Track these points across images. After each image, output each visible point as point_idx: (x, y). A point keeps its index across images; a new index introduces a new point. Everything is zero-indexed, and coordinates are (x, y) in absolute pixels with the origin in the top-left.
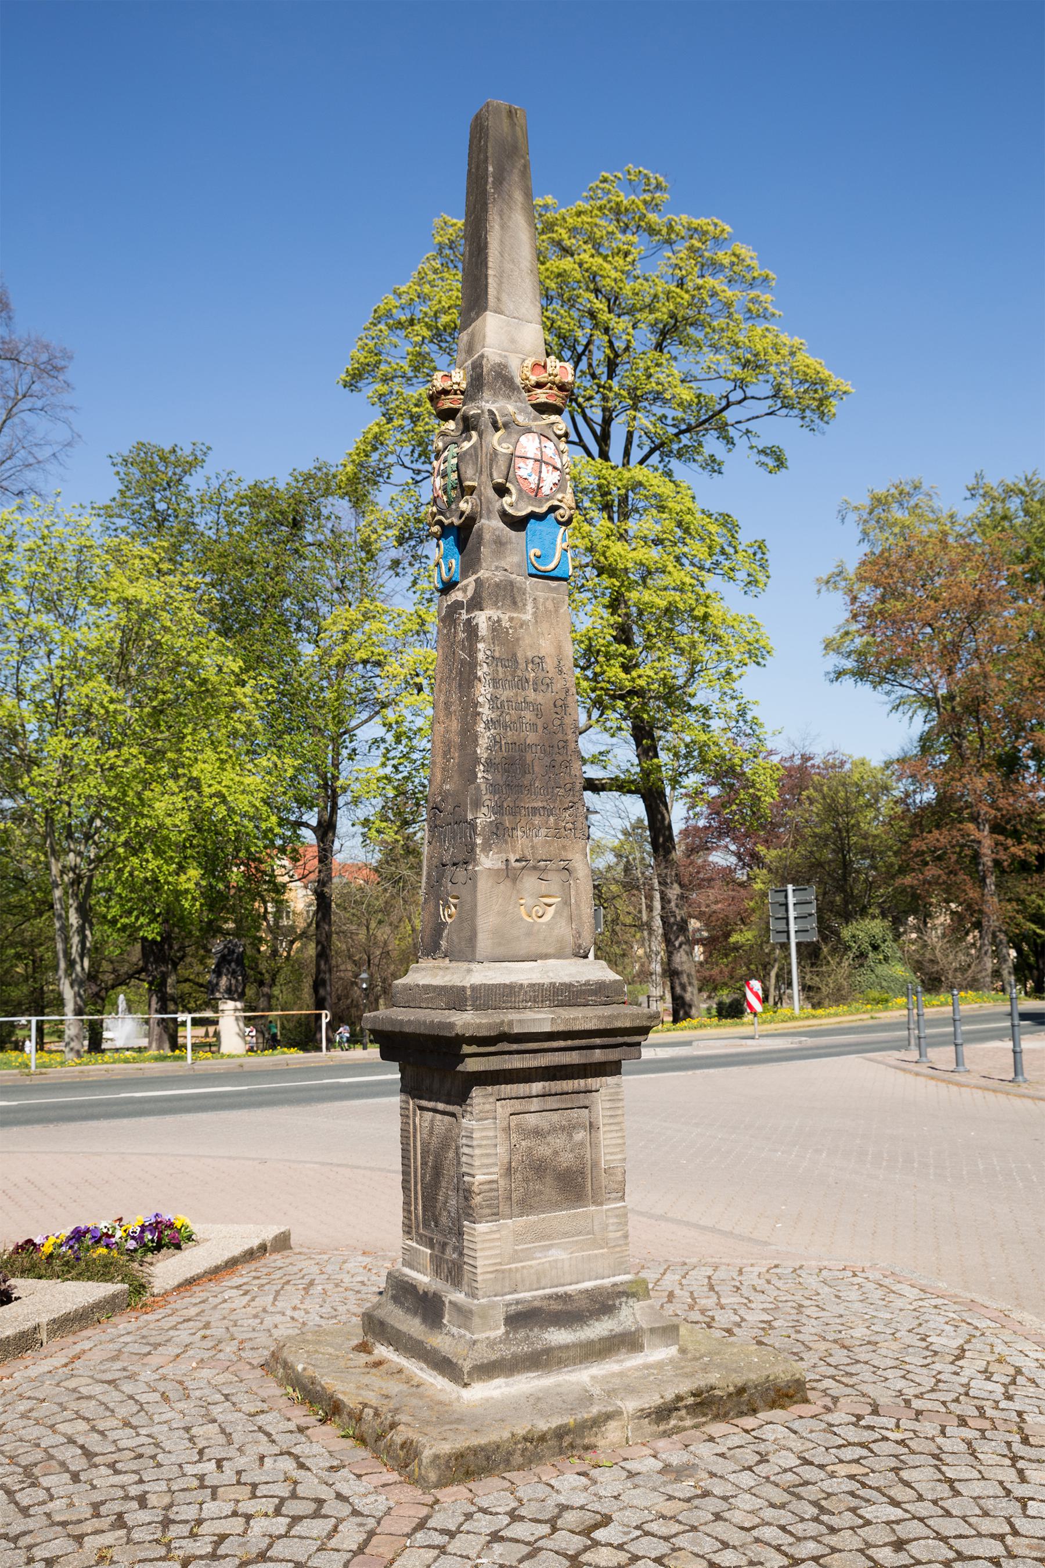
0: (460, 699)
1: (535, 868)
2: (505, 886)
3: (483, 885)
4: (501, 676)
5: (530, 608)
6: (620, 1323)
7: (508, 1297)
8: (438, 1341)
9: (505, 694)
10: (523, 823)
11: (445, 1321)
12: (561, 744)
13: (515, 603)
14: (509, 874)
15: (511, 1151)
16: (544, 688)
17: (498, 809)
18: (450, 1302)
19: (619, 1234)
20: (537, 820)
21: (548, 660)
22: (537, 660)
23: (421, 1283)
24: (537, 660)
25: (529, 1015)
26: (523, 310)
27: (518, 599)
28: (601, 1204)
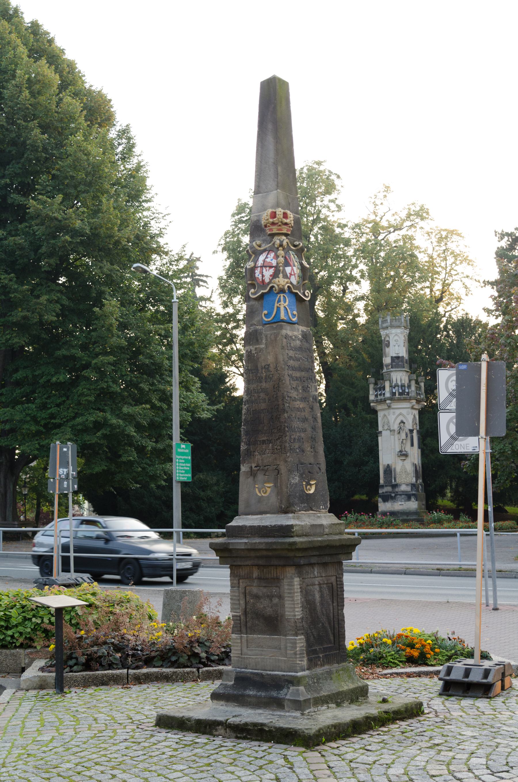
1: (263, 470)
2: (250, 480)
3: (242, 479)
10: (258, 448)
13: (257, 340)
14: (252, 474)
17: (248, 444)
19: (292, 652)
21: (271, 366)
22: (267, 367)
28: (286, 636)
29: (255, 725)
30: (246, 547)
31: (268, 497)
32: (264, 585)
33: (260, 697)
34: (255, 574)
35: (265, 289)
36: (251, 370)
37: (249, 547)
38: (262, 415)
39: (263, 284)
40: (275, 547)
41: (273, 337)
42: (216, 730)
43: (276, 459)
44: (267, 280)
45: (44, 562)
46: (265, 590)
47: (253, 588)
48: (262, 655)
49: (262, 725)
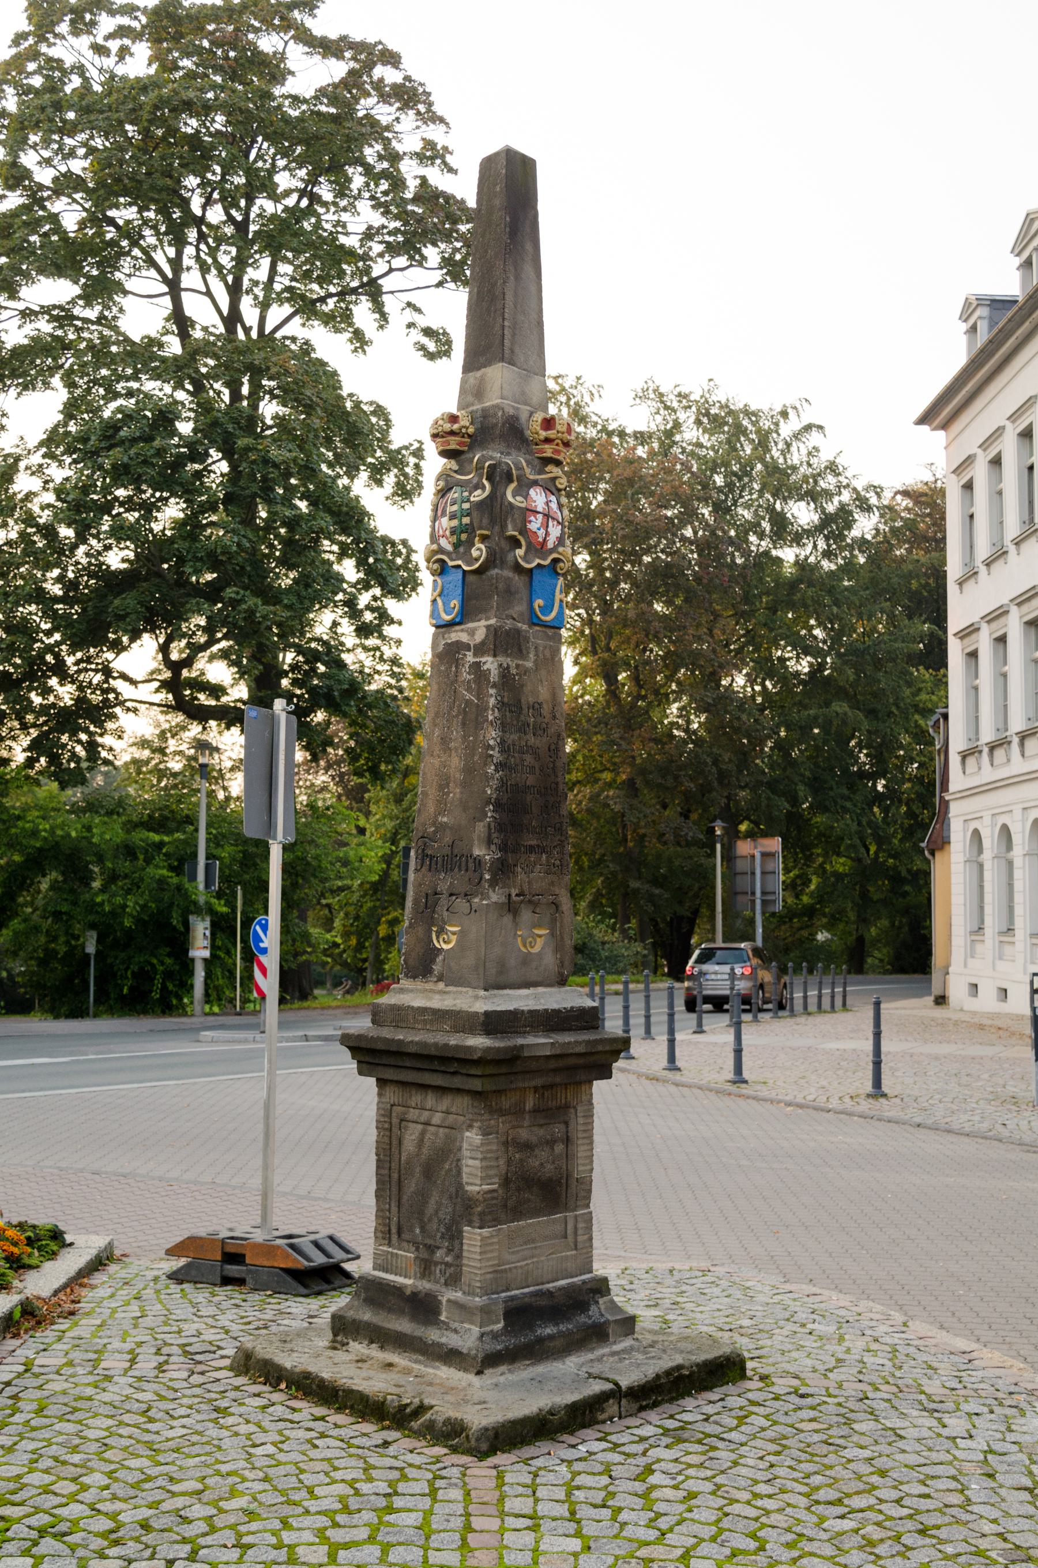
0: (465, 738)
1: (530, 902)
6: (590, 1317)
7: (503, 1295)
8: (433, 1335)
9: (512, 737)
11: (443, 1318)
13: (520, 651)
15: (509, 1162)
18: (449, 1301)
20: (533, 857)
21: (545, 706)
23: (406, 1286)
25: (530, 1040)
28: (575, 1210)
29: (668, 1373)
30: (553, 1052)
31: (539, 954)
32: (542, 1122)
33: (570, 1333)
34: (529, 1104)
35: (544, 559)
36: (509, 705)
37: (558, 1052)
38: (529, 798)
39: (539, 548)
40: (600, 1048)
42: (603, 1411)
43: (552, 883)
44: (550, 545)
46: (541, 1132)
47: (520, 1130)
48: (533, 1257)
49: (679, 1367)
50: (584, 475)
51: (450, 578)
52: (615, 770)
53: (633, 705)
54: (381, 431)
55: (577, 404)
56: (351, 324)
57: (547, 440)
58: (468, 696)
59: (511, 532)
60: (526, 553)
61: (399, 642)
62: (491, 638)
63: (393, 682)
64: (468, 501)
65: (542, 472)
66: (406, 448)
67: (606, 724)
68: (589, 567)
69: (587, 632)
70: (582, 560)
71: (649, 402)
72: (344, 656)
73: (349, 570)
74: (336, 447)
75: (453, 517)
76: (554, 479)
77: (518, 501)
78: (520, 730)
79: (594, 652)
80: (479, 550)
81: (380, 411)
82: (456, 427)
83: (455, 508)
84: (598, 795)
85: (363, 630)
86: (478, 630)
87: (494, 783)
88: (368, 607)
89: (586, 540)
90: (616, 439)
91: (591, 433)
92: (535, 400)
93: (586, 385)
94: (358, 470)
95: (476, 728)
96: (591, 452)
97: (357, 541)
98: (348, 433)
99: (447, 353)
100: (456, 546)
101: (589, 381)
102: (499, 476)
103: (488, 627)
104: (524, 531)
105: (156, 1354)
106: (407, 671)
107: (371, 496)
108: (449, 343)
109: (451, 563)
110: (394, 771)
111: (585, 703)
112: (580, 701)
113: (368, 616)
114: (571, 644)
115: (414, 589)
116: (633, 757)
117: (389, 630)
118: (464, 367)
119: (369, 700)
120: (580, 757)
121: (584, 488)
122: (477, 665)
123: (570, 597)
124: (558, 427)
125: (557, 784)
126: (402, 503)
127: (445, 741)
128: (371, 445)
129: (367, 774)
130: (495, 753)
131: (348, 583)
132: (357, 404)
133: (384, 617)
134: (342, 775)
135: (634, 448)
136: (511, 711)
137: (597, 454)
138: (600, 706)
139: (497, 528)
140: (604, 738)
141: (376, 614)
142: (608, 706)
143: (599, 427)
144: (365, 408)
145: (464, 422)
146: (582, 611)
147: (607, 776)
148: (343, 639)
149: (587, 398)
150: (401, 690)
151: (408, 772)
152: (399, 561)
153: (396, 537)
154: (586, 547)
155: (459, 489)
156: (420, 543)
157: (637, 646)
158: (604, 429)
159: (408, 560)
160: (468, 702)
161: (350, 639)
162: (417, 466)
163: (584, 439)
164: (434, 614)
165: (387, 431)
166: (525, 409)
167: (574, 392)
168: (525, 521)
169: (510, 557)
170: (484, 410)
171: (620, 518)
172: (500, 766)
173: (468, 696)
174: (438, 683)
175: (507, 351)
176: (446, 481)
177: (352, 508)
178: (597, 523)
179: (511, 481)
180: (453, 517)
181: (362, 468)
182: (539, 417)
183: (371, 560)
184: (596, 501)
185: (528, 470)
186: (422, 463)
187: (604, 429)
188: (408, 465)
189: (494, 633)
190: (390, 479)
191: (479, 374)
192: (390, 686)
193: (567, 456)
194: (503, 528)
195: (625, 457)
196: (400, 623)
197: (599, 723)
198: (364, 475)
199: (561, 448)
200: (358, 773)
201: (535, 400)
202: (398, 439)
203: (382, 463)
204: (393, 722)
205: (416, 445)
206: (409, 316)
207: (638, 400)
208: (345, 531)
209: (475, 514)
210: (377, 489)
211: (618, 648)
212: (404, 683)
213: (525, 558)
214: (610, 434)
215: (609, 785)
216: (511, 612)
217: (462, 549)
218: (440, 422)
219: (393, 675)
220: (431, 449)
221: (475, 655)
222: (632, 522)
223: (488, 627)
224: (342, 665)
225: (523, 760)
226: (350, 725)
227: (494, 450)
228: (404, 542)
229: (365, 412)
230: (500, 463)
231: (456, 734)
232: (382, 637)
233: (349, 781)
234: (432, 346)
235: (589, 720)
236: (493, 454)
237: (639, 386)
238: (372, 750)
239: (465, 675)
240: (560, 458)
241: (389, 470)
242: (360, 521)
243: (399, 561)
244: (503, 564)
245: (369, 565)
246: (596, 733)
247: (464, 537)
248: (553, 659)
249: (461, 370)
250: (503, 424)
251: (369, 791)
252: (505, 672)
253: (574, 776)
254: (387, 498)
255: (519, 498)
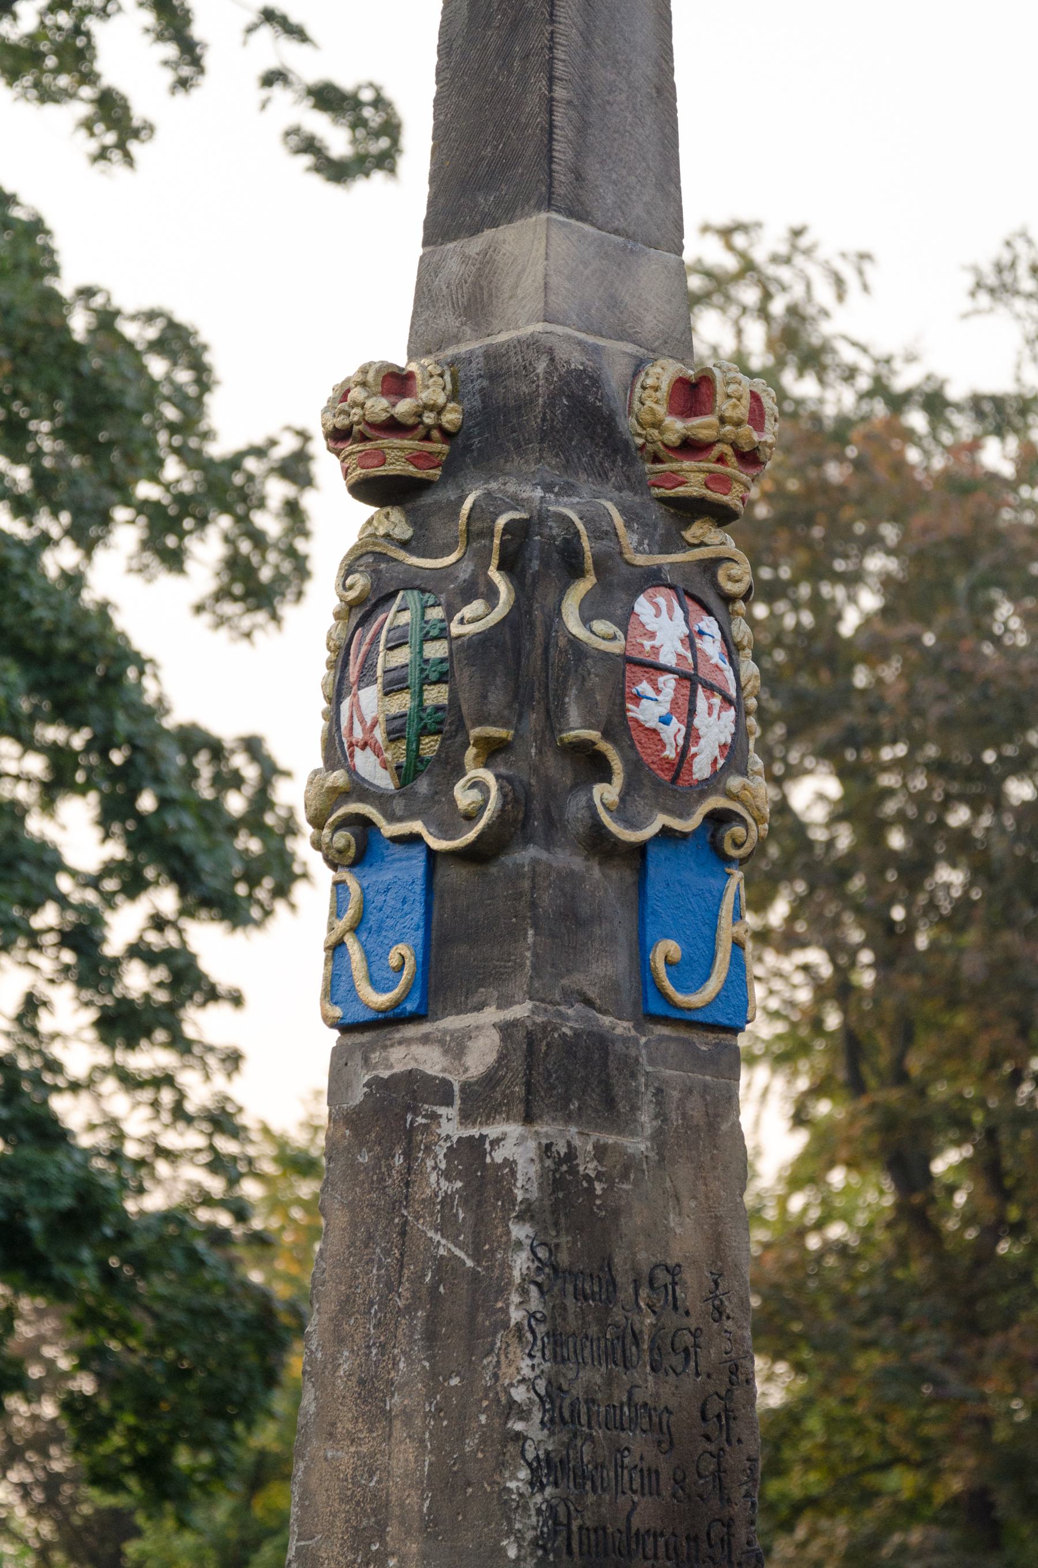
0: (434, 1378)
4: (573, 1323)
5: (645, 1118)
12: (718, 1530)
13: (610, 1102)
16: (677, 1360)
21: (688, 1276)
24: (663, 1277)
26: (639, 211)
27: (619, 1091)
39: (672, 783)
41: (696, 1109)
44: (701, 768)
45: (41, 1042)
50: (815, 531)
51: (387, 876)
52: (928, 1460)
53: (983, 1255)
54: (179, 398)
55: (793, 310)
56: (89, 78)
57: (690, 447)
58: (445, 1247)
59: (578, 731)
60: (623, 797)
61: (233, 1060)
62: (517, 1062)
63: (215, 1185)
64: (443, 634)
65: (671, 543)
66: (259, 452)
67: (898, 1315)
68: (835, 819)
69: (833, 1020)
70: (814, 793)
71: (1019, 305)
72: (59, 1104)
73: (77, 834)
74: (39, 453)
75: (393, 686)
76: (711, 566)
77: (600, 635)
78: (609, 1356)
79: (856, 1086)
80: (478, 789)
81: (177, 341)
82: (404, 407)
83: (402, 656)
84: (874, 1543)
85: (122, 1024)
86: (477, 1037)
87: (529, 1524)
88: (138, 951)
89: (826, 733)
90: (917, 420)
91: (838, 400)
92: (651, 323)
93: (821, 254)
94: (106, 520)
95: (470, 1349)
96: (841, 458)
97: (101, 744)
98: (79, 406)
99: (386, 161)
100: (405, 775)
101: (831, 240)
102: (539, 558)
103: (506, 1029)
104: (618, 726)
105: (666, 1407)
106: (261, 1150)
107: (152, 607)
108: (391, 129)
109: (389, 830)
110: (218, 1471)
111: (828, 1247)
112: (813, 1242)
113: (137, 981)
114: (785, 1056)
115: (281, 891)
116: (986, 1423)
117: (203, 1023)
118: (430, 225)
119: (141, 1243)
120: (813, 1423)
121: (818, 571)
122: (472, 1150)
123: (779, 912)
124: (724, 406)
125: (729, 1523)
126: (246, 622)
127: (370, 1389)
128: (151, 445)
129: (132, 1482)
130: (530, 1428)
131: (74, 873)
132: (106, 320)
133: (186, 979)
134: (52, 1483)
135: (975, 446)
136: (580, 1295)
137: (859, 465)
138: (875, 1258)
139: (533, 719)
140: (892, 1360)
141: (161, 973)
142: (902, 1257)
143: (864, 383)
144: (130, 330)
145: (432, 392)
146: (815, 956)
147: (902, 1482)
148: (56, 1050)
149: (824, 294)
150: (241, 1212)
151: (266, 1471)
152: (236, 803)
153: (226, 728)
154: (828, 753)
155: (413, 598)
156: (300, 756)
157: (993, 1064)
158: (879, 388)
159: (262, 801)
160: (444, 1267)
161: (79, 1052)
162: (293, 510)
163: (816, 418)
164: (336, 986)
165: (199, 401)
166: (618, 353)
167: (784, 273)
168: (621, 697)
169: (574, 809)
170: (491, 355)
171: (932, 661)
172: (547, 1469)
173: (445, 1247)
174: (351, 1207)
175: (562, 174)
176: (376, 573)
177: (87, 642)
178: (861, 678)
179: (576, 572)
180: (393, 686)
181: (121, 514)
182: (663, 374)
183: (147, 802)
184: (858, 610)
185: (628, 539)
186: (309, 501)
187: (879, 388)
188: (261, 504)
189: (525, 1044)
190: (207, 550)
191: (475, 245)
192: (207, 1200)
193: (755, 497)
194: (554, 717)
195: (946, 473)
196: (237, 1000)
197: (876, 1311)
198: (126, 534)
199: (732, 468)
200: (103, 1478)
201: (651, 323)
202: (232, 424)
203: (181, 499)
204: (216, 1314)
205: (288, 445)
206: (272, 49)
207: (984, 299)
208: (66, 712)
209: (464, 676)
210: (166, 581)
211: (933, 1072)
212: (251, 1189)
213: (622, 811)
214: (898, 402)
215: (909, 1511)
216: (578, 980)
217: (423, 786)
218: (357, 394)
219: (218, 1164)
220: (328, 468)
221: (466, 1117)
222: (969, 677)
223: (506, 1029)
224: (51, 1133)
225: (622, 1451)
226: (80, 1324)
227: (522, 478)
228: (252, 746)
229: (129, 345)
230: (542, 518)
231: (407, 1367)
232: (180, 1044)
233: (74, 1502)
234: (338, 140)
235: (843, 1303)
236: (521, 491)
237: (987, 252)
238: (147, 1403)
239: (436, 1181)
240: (731, 499)
241: (203, 522)
242: (113, 681)
243: (236, 803)
244: (553, 828)
245: (140, 818)
246: (866, 1345)
247: (430, 746)
248: (712, 1127)
249: (418, 234)
250: (552, 401)
251: (137, 1533)
252: (560, 1171)
253: (799, 1482)
254: (199, 609)
255: (601, 626)
